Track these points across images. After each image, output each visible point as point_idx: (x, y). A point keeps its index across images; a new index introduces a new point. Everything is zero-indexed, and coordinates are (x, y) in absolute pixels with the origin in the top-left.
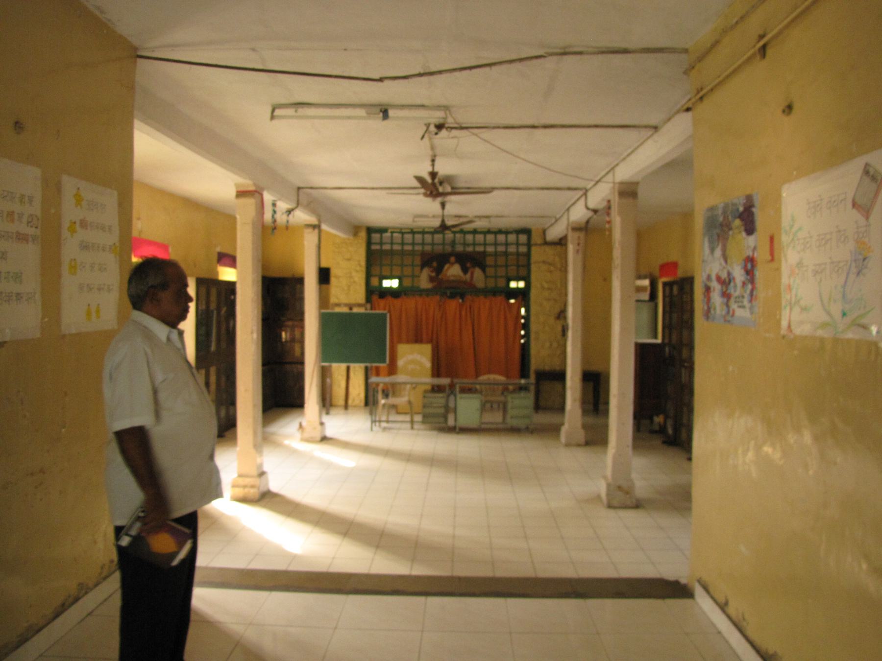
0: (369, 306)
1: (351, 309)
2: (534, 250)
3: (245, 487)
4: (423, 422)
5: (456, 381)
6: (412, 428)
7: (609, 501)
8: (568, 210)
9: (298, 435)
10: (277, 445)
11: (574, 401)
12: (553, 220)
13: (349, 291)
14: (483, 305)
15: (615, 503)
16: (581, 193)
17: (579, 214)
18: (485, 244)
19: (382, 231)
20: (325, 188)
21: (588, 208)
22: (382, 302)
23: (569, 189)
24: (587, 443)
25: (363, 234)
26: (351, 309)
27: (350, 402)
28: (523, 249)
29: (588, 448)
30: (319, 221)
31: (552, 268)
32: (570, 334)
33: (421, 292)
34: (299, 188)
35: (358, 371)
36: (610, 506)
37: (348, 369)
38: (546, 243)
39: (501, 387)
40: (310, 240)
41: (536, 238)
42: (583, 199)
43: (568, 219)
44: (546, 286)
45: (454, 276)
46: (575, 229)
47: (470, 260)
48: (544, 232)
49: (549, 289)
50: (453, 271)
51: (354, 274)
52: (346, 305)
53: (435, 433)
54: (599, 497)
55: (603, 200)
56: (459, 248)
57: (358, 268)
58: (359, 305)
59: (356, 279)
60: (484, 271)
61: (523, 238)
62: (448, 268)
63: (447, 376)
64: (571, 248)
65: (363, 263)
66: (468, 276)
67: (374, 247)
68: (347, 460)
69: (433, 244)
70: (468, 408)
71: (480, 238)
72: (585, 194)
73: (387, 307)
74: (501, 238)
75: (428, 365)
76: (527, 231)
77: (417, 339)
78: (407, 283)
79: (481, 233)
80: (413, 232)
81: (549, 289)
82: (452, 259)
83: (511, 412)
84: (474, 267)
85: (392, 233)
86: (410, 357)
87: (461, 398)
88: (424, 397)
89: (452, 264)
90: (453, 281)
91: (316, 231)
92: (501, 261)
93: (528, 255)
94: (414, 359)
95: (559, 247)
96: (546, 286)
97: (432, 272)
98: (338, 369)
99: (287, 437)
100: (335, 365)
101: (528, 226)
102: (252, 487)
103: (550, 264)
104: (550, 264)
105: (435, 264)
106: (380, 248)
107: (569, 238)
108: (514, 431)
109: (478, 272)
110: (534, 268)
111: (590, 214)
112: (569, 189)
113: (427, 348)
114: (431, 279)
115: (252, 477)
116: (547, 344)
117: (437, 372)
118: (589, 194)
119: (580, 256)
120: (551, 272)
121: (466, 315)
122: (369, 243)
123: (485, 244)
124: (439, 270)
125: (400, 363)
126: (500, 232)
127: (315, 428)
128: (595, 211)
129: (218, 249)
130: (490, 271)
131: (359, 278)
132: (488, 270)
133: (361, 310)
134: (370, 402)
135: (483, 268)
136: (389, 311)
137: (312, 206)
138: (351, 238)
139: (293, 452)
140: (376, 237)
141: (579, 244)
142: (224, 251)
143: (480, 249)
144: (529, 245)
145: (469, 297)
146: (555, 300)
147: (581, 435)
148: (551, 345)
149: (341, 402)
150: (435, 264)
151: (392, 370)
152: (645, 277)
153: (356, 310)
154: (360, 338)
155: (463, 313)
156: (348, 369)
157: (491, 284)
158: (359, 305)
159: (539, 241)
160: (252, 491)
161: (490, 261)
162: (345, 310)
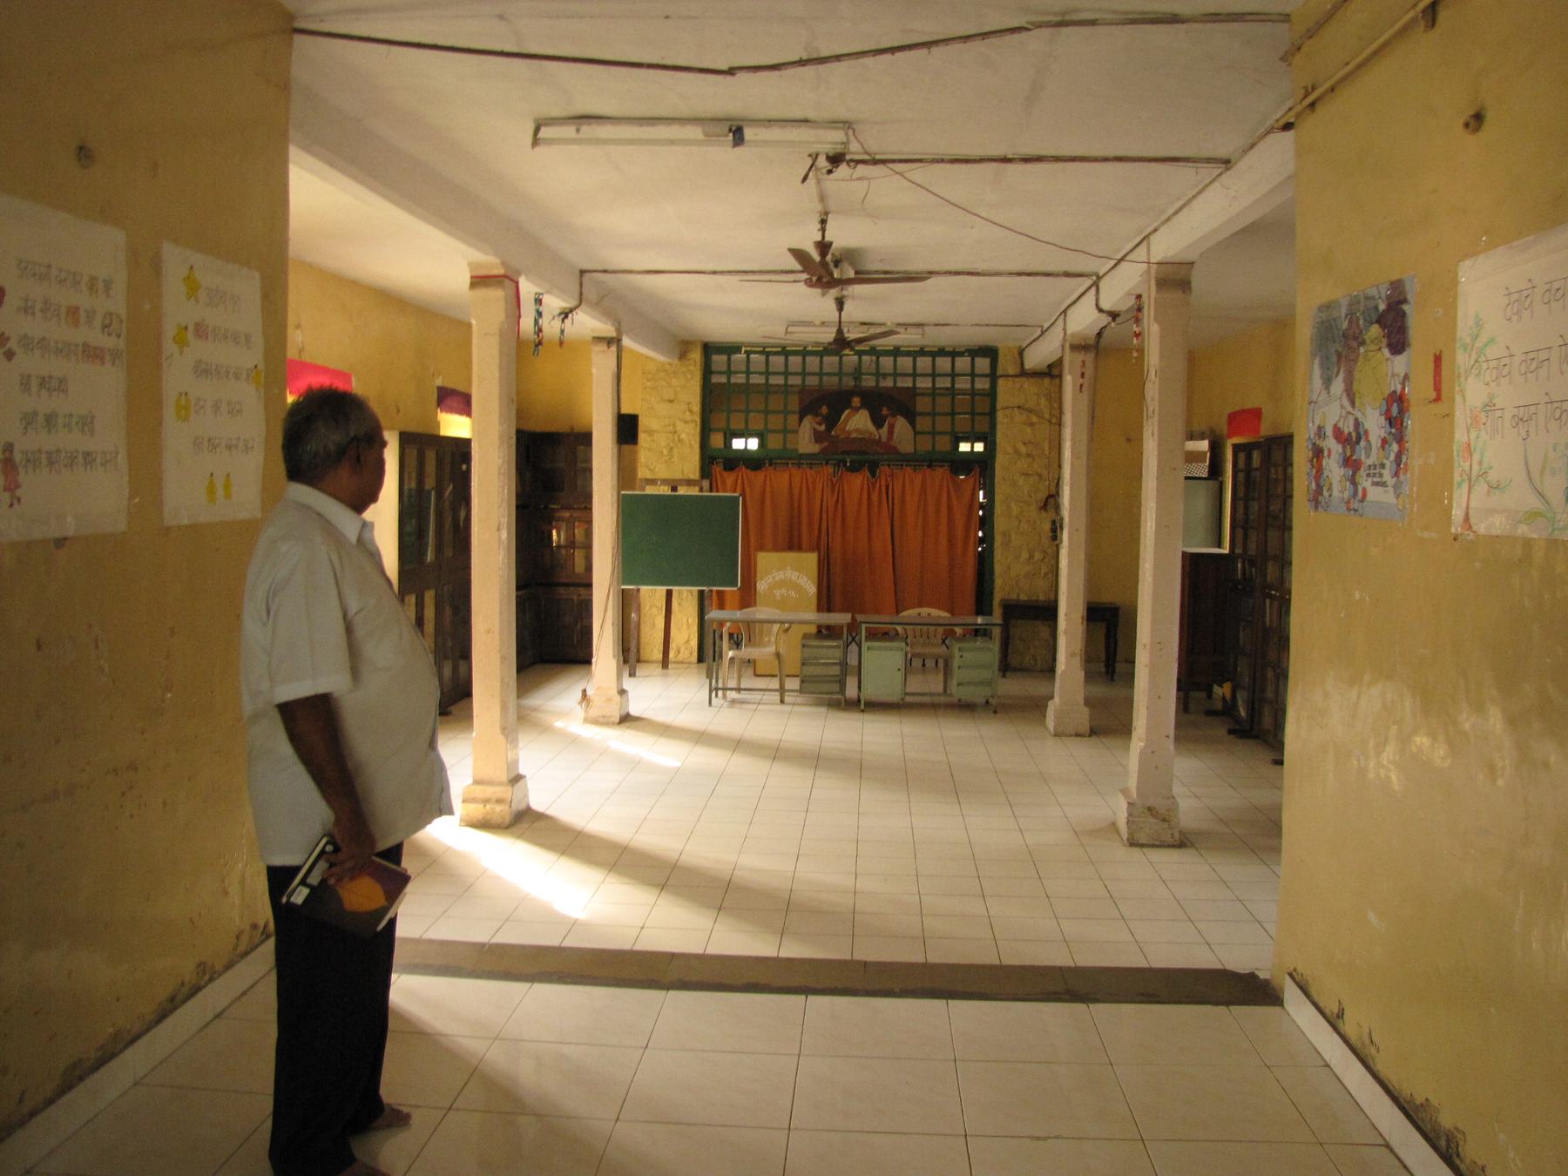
0: (706, 484)
1: (674, 489)
3: (486, 801)
4: (801, 691)
5: (859, 618)
6: (782, 701)
7: (1131, 833)
8: (1065, 312)
9: (580, 712)
10: (544, 729)
13: (671, 456)
14: (910, 483)
16: (1089, 282)
17: (1084, 319)
19: (730, 349)
20: (631, 272)
21: (1101, 310)
22: (730, 478)
23: (1067, 274)
24: (1093, 732)
25: (696, 355)
26: (674, 489)
27: (671, 655)
28: (982, 384)
29: (1094, 738)
30: (619, 331)
31: (1035, 419)
32: (1065, 535)
33: (800, 460)
34: (582, 272)
35: (686, 600)
36: (1133, 843)
37: (669, 594)
38: (1023, 373)
39: (941, 630)
40: (601, 365)
41: (1006, 365)
43: (1065, 330)
44: (1023, 449)
45: (857, 430)
46: (1076, 348)
48: (1021, 352)
49: (1028, 455)
50: (858, 422)
51: (680, 426)
52: (665, 482)
53: (823, 710)
56: (868, 382)
57: (688, 416)
58: (689, 483)
59: (683, 436)
60: (913, 424)
61: (983, 364)
62: (847, 420)
65: (697, 408)
67: (715, 379)
68: (666, 755)
70: (882, 666)
71: (905, 363)
72: (1096, 284)
73: (739, 488)
75: (812, 589)
76: (990, 352)
77: (793, 544)
78: (775, 442)
79: (908, 354)
80: (785, 352)
81: (1028, 455)
82: (856, 401)
85: (748, 353)
86: (779, 576)
89: (857, 409)
91: (614, 348)
92: (943, 404)
93: (992, 394)
94: (787, 580)
95: (1047, 380)
96: (1023, 449)
98: (652, 596)
99: (562, 714)
100: (645, 589)
102: (499, 801)
103: (1031, 411)
104: (1031, 411)
105: (824, 410)
106: (726, 380)
107: (1066, 364)
109: (901, 424)
110: (1000, 415)
111: (1105, 319)
112: (1067, 274)
113: (810, 560)
114: (818, 437)
115: (500, 784)
116: (1025, 555)
117: (826, 602)
118: (1102, 284)
119: (1085, 398)
120: (1031, 424)
122: (707, 372)
123: (914, 375)
124: (832, 421)
125: (762, 586)
126: (942, 352)
127: (609, 700)
129: (439, 382)
130: (923, 423)
131: (690, 434)
133: (694, 491)
134: (706, 654)
135: (911, 417)
136: (743, 494)
137: (605, 303)
138: (676, 361)
139: (573, 741)
140: (719, 360)
141: (1083, 375)
142: (450, 385)
144: (993, 376)
146: (1040, 475)
147: (1083, 717)
148: (1031, 557)
149: (660, 656)
150: (824, 410)
151: (748, 597)
153: (682, 491)
154: (691, 540)
155: (875, 498)
156: (669, 594)
157: (925, 445)
158: (689, 483)
160: (498, 808)
161: (922, 404)
162: (665, 490)
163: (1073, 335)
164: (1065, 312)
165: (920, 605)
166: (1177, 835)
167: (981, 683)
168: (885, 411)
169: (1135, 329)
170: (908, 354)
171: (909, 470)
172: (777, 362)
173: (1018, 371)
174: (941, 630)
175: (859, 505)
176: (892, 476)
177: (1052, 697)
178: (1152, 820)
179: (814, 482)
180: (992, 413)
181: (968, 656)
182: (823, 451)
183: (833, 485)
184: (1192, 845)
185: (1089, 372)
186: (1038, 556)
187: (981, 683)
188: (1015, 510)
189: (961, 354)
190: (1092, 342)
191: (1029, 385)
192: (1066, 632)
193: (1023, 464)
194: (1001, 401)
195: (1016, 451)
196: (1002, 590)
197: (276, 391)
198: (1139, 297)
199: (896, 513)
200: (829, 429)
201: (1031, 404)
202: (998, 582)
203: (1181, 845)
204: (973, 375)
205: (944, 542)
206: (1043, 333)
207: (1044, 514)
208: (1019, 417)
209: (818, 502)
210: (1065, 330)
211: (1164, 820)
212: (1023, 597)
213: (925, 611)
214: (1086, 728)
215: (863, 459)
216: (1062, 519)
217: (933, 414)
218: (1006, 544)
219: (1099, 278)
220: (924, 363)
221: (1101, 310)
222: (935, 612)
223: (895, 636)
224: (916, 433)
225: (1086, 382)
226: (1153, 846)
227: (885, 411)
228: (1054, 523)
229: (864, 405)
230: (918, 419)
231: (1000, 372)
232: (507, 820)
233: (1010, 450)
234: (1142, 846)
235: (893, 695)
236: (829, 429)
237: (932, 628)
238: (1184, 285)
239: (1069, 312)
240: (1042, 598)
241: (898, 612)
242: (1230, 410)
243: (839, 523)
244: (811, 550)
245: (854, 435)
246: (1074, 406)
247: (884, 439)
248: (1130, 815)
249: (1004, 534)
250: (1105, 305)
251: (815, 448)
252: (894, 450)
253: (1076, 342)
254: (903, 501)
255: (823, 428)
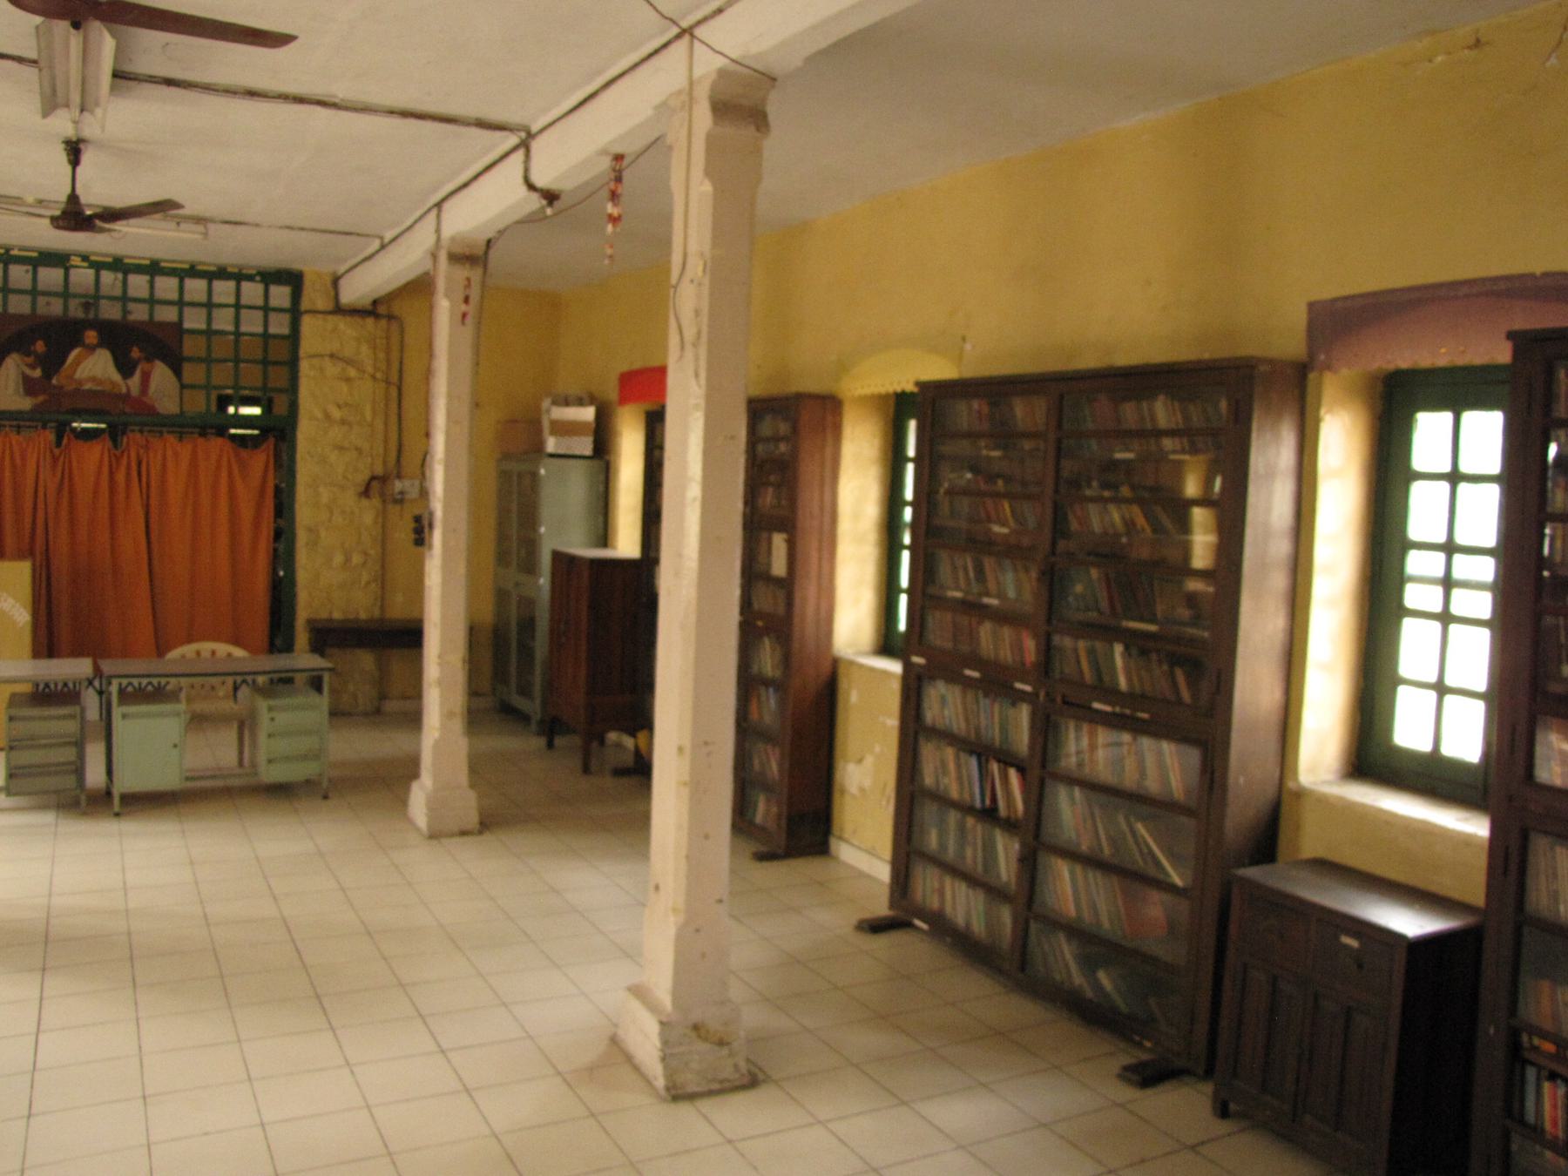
2: (307, 324)
5: (107, 666)
7: (670, 1073)
8: (439, 205)
11: (448, 715)
12: (376, 244)
14: (174, 460)
15: (692, 1084)
16: (513, 140)
17: (492, 203)
18: (181, 303)
21: (531, 187)
23: (482, 124)
24: (487, 823)
28: (280, 325)
29: (487, 837)
31: (352, 373)
32: (437, 537)
36: (677, 1094)
38: (339, 310)
39: (230, 680)
41: (314, 297)
42: (519, 156)
43: (438, 231)
44: (337, 414)
45: (93, 379)
46: (454, 258)
47: (136, 342)
48: (336, 281)
49: (343, 422)
50: (94, 367)
53: (49, 817)
54: (617, 1050)
55: (603, 152)
56: (110, 312)
60: (178, 372)
61: (280, 295)
62: (78, 362)
63: (77, 652)
64: (444, 308)
66: (135, 381)
69: (34, 292)
70: (150, 744)
71: (167, 287)
72: (525, 145)
74: (224, 290)
75: (22, 616)
76: (293, 279)
79: (172, 272)
81: (343, 422)
82: (91, 336)
83: (265, 746)
84: (149, 359)
87: (124, 716)
88: (11, 719)
89: (91, 349)
90: (93, 394)
92: (221, 349)
93: (294, 337)
95: (370, 321)
96: (337, 414)
97: (33, 367)
101: (296, 266)
103: (348, 362)
104: (348, 362)
105: (40, 346)
107: (441, 284)
108: (280, 793)
109: (161, 374)
110: (304, 366)
111: (536, 202)
112: (482, 124)
114: (30, 387)
116: (338, 559)
117: (46, 644)
118: (535, 145)
119: (468, 332)
120: (348, 380)
121: (128, 486)
123: (181, 303)
124: (52, 362)
126: (222, 273)
128: (551, 197)
130: (192, 373)
132: (187, 369)
135: (176, 365)
141: (466, 300)
143: (168, 315)
144: (295, 313)
145: (134, 439)
146: (359, 450)
147: (467, 806)
148: (348, 560)
150: (40, 346)
152: (580, 402)
155: (121, 477)
157: (199, 403)
159: (322, 303)
161: (190, 347)
163: (453, 239)
164: (439, 205)
165: (190, 640)
166: (742, 1064)
167: (304, 758)
168: (136, 353)
169: (610, 209)
170: (172, 272)
171: (172, 439)
172: (252, 292)
173: (330, 306)
174: (230, 680)
175: (96, 492)
176: (147, 447)
177: (415, 775)
178: (702, 1046)
179: (23, 458)
180: (293, 363)
181: (283, 718)
182: (36, 409)
183: (55, 460)
184: (768, 1079)
185: (475, 294)
186: (356, 559)
187: (304, 758)
188: (325, 495)
189: (250, 278)
190: (480, 251)
191: (342, 323)
192: (440, 683)
193: (336, 433)
194: (308, 344)
195: (327, 416)
196: (308, 605)
197: (917, 660)
198: (619, 158)
199: (154, 502)
200: (48, 375)
201: (348, 352)
202: (302, 597)
203: (751, 1081)
204: (266, 309)
205: (223, 539)
206: (383, 247)
207: (365, 502)
208: (332, 369)
209: (30, 482)
210: (438, 231)
211: (721, 1043)
212: (337, 615)
213: (206, 647)
214: (472, 819)
215: (124, 420)
216: (431, 514)
217: (208, 360)
218: (314, 544)
219: (531, 135)
220: (196, 288)
221: (531, 187)
222: (223, 649)
223: (172, 697)
224: (183, 387)
225: (471, 309)
226: (711, 1093)
227: (136, 353)
228: (418, 519)
229: (102, 343)
230: (186, 367)
231: (305, 304)
232: (1194, 755)
233: (320, 415)
234: (692, 1097)
235: (169, 780)
236: (48, 375)
237: (220, 679)
238: (757, 118)
239: (447, 206)
240: (363, 616)
241: (161, 651)
242: (625, 368)
243: (64, 514)
244: (20, 556)
245: (87, 386)
246: (451, 344)
247: (135, 391)
248: (665, 1043)
249: (310, 530)
250: (540, 180)
251: (26, 404)
252: (151, 411)
253: (458, 250)
254: (163, 481)
255: (37, 373)
